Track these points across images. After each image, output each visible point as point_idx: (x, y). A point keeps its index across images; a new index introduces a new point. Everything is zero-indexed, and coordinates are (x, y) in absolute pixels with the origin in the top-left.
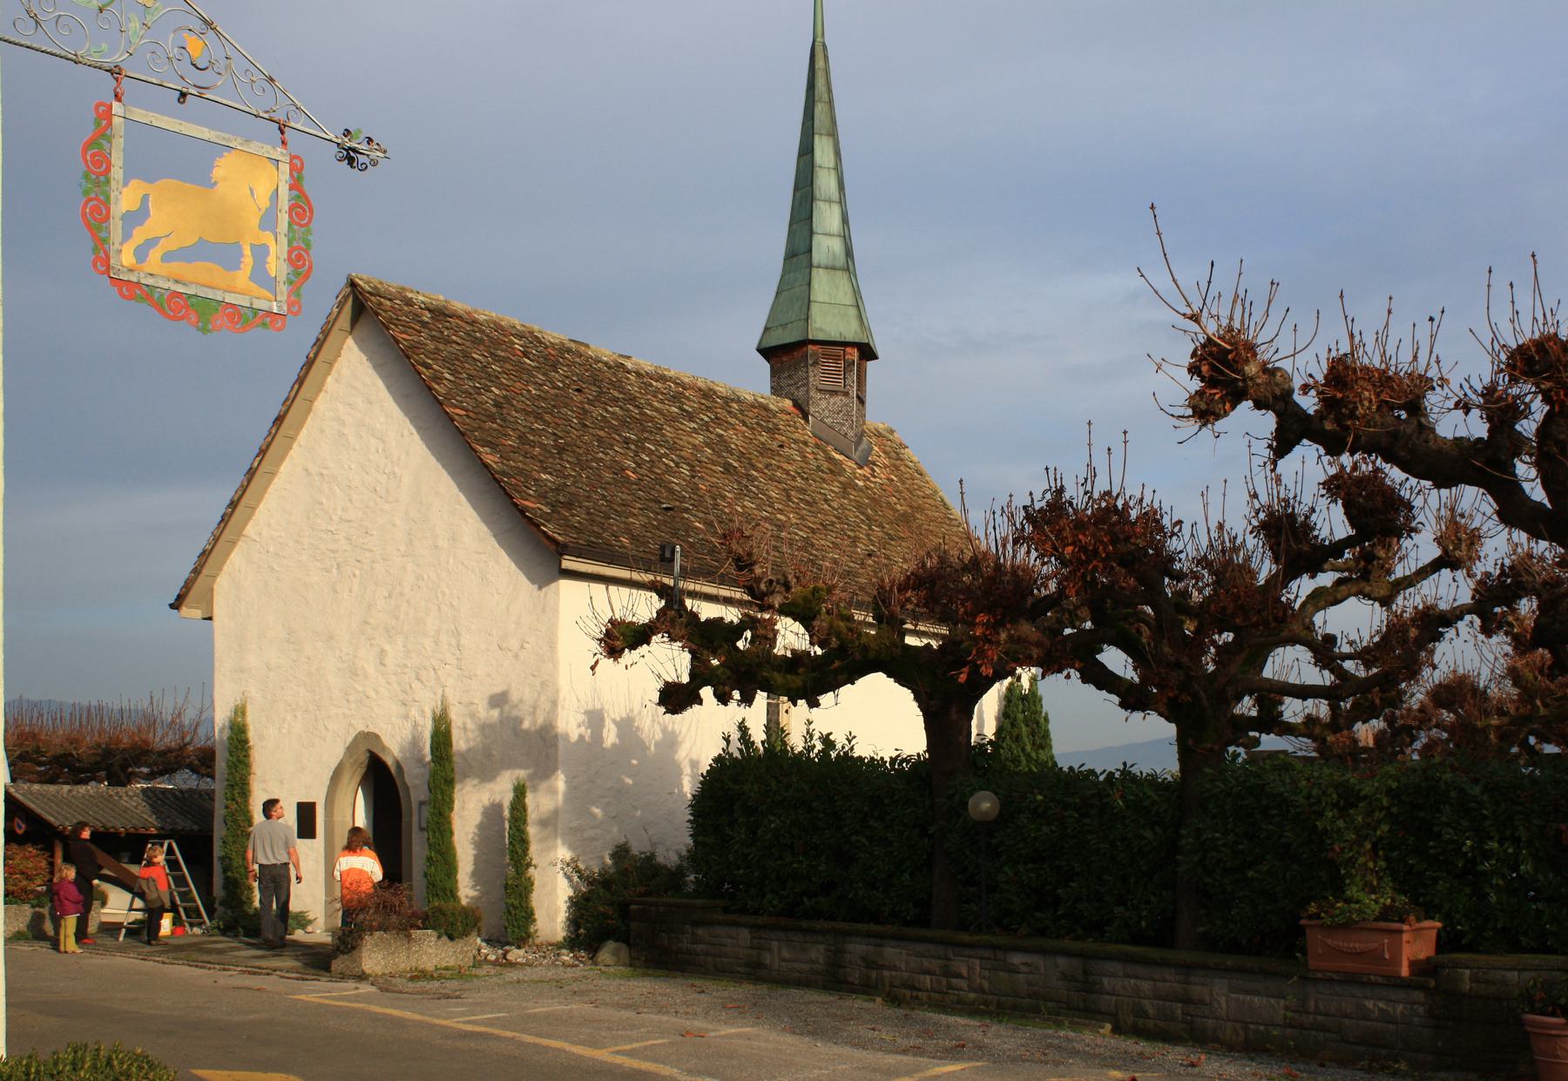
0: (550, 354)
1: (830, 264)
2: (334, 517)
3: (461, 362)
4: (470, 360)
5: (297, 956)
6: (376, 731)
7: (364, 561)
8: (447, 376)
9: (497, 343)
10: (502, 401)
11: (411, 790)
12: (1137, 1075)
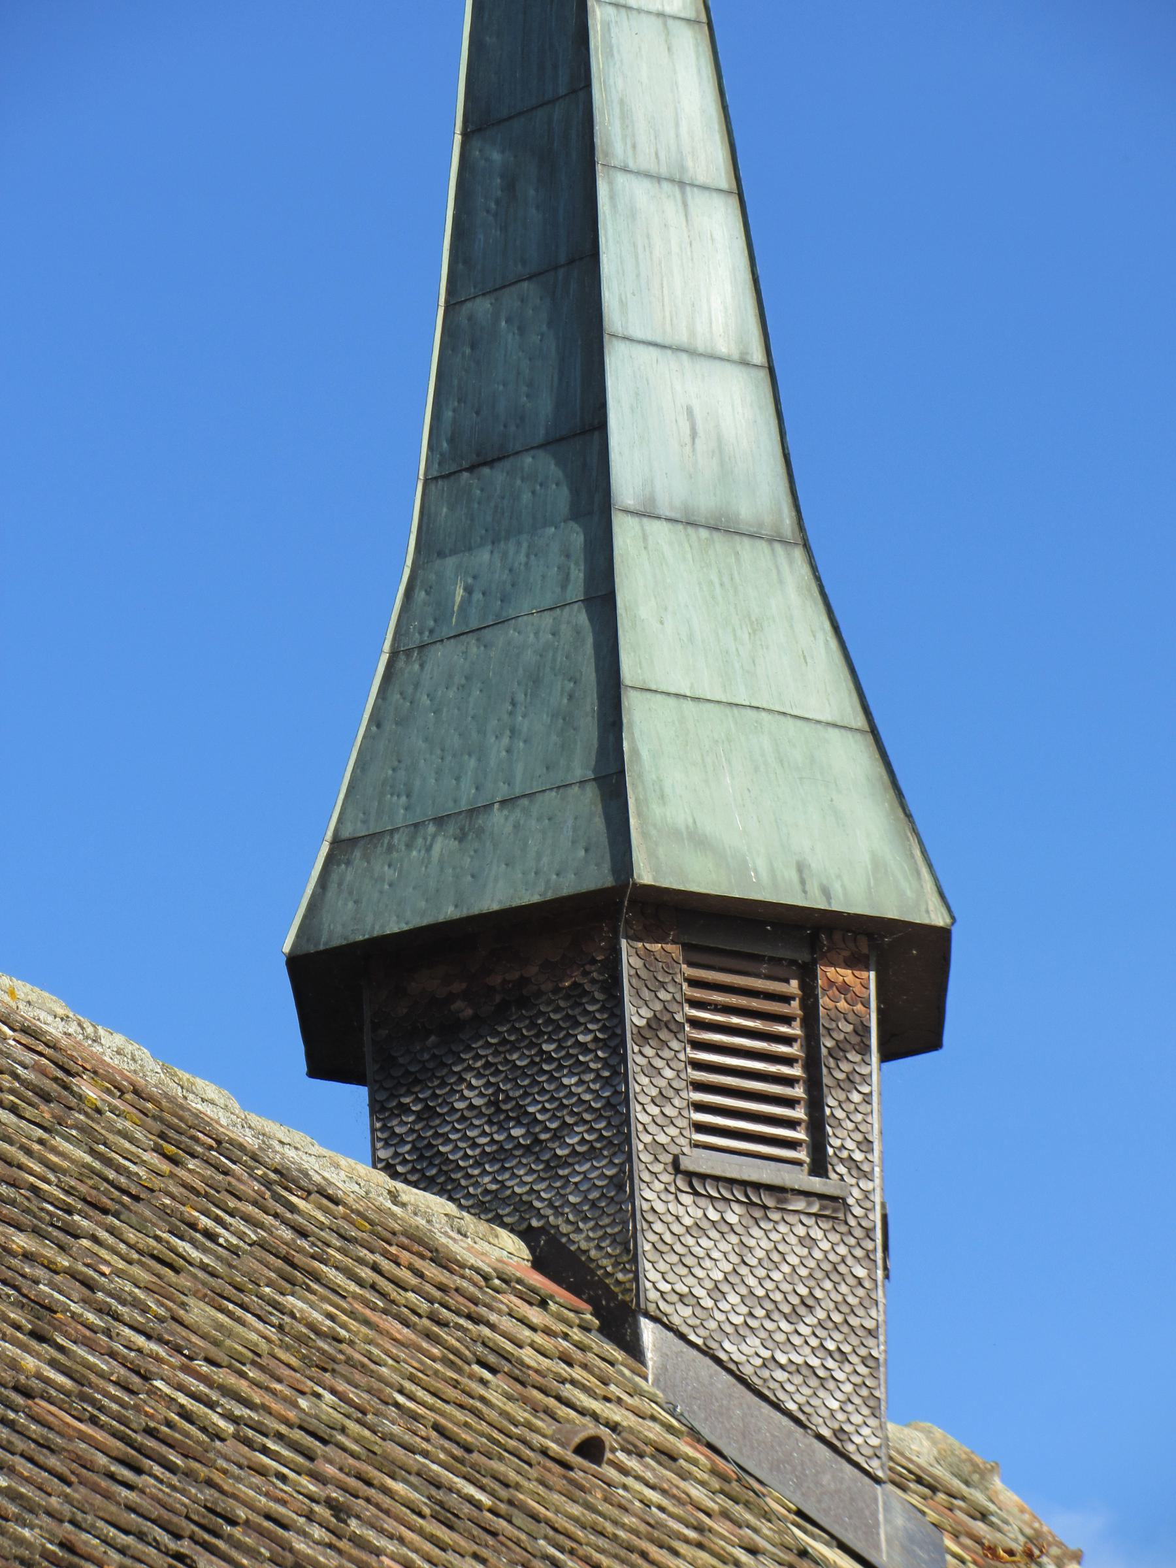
1: (705, 503)
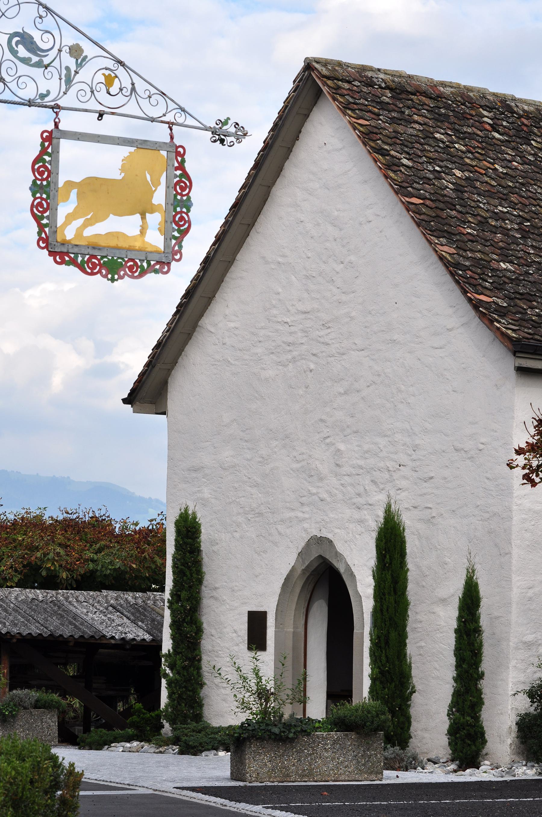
0: (523, 124)
2: (290, 308)
3: (422, 144)
4: (431, 142)
6: (330, 536)
7: (320, 355)
8: (405, 161)
9: (463, 117)
10: (463, 183)
11: (363, 599)
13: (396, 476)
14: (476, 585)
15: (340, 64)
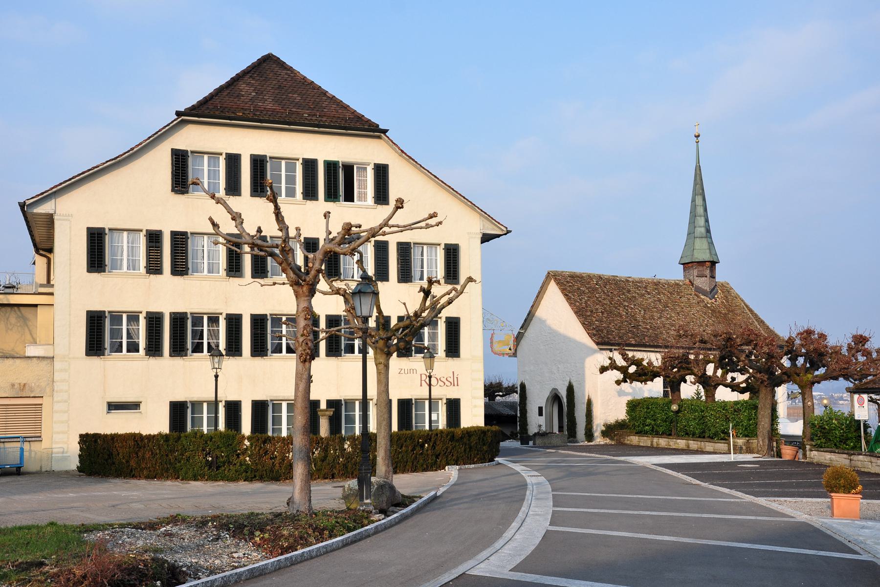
1: (701, 236)
4: (580, 291)
5: (584, 324)
12: (586, 443)
13: (572, 373)
14: (590, 400)
15: (557, 271)
